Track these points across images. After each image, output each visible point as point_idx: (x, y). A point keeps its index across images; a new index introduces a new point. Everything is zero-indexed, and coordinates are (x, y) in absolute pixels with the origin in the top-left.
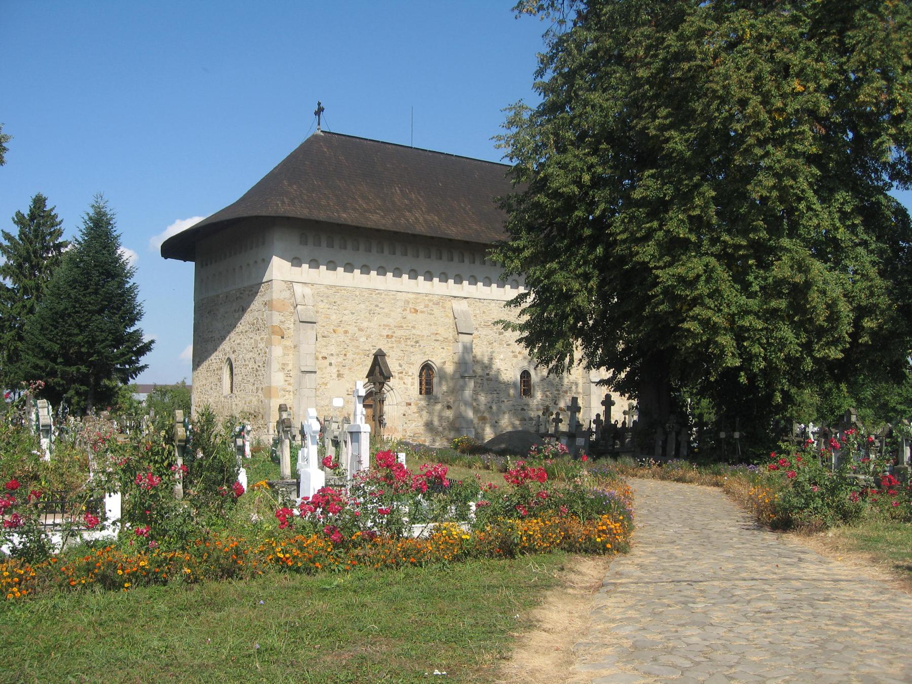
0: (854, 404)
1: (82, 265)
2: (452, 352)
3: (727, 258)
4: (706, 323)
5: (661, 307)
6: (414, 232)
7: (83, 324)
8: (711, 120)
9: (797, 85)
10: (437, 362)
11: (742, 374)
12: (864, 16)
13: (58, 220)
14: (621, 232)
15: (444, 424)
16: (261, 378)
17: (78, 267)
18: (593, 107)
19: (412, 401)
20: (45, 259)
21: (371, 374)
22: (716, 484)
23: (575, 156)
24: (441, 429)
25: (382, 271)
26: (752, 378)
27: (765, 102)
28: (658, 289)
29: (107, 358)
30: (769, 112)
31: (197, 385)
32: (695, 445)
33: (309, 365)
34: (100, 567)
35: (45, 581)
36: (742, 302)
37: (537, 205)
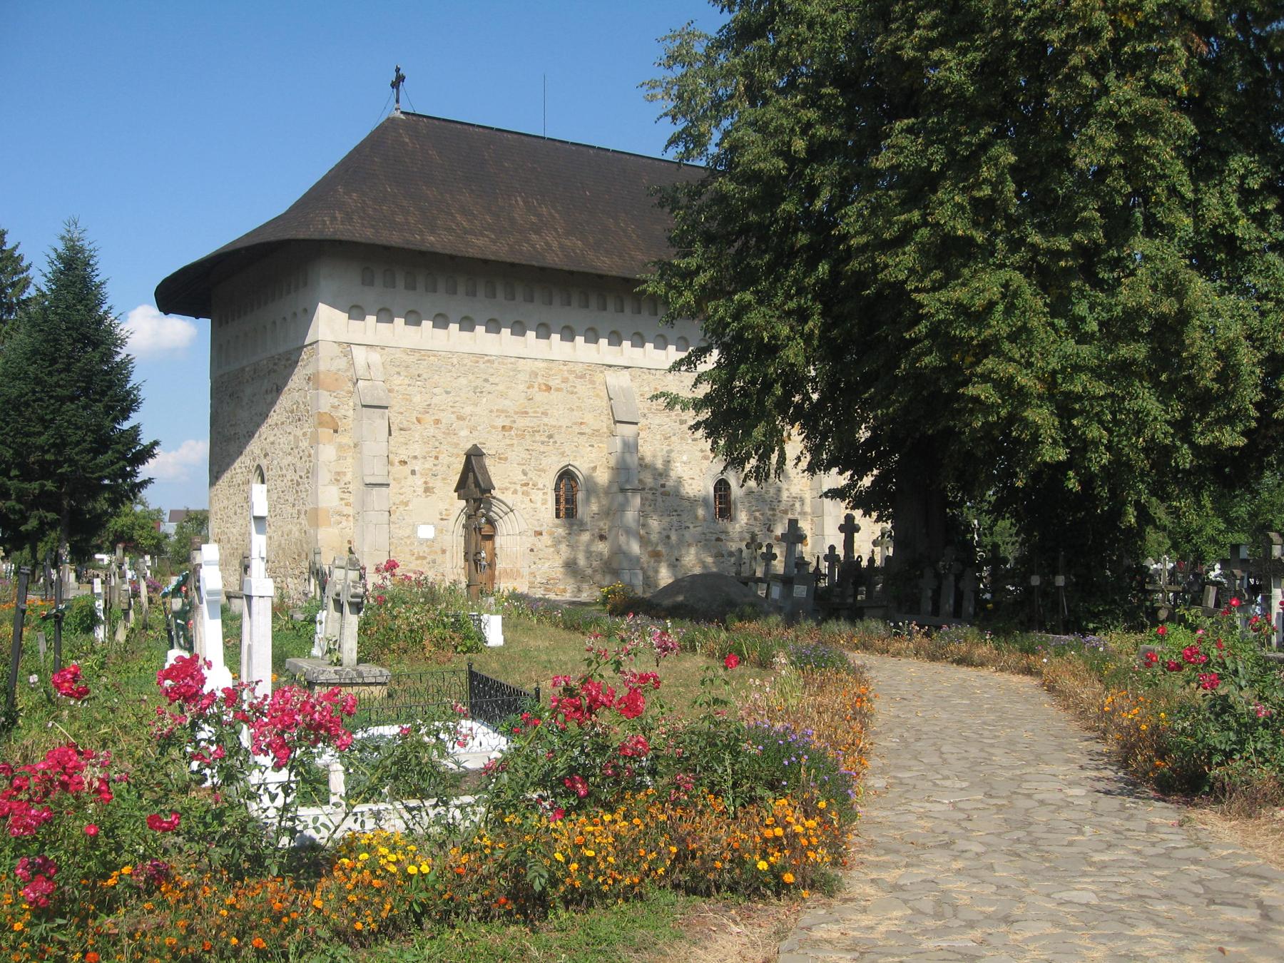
0: (1222, 526)
2: (605, 451)
3: (1045, 275)
4: (1005, 386)
5: (927, 360)
6: (541, 264)
7: (48, 417)
10: (582, 466)
11: (1071, 474)
13: (24, 264)
14: (857, 233)
15: (595, 563)
18: (811, 26)
19: (544, 529)
22: (1028, 671)
23: (781, 109)
24: (589, 571)
26: (1088, 481)
28: (922, 328)
31: (216, 507)
32: (988, 596)
33: (377, 472)
37: (722, 198)
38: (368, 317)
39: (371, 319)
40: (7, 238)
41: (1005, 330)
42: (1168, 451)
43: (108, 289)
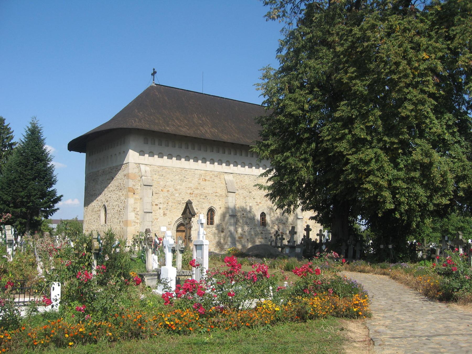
1: (24, 154)
2: (224, 202)
3: (386, 150)
4: (376, 185)
5: (351, 176)
8: (379, 73)
9: (425, 55)
12: (459, 19)
13: (11, 131)
16: (122, 215)
17: (22, 155)
18: (310, 68)
20: (4, 151)
21: (184, 213)
22: (384, 274)
25: (188, 159)
27: (409, 63)
28: (349, 166)
29: (37, 204)
30: (411, 69)
31: (86, 219)
34: (54, 334)
35: (17, 342)
36: (395, 173)
37: (278, 121)
38: (146, 155)
39: (147, 156)
40: (5, 121)
41: (376, 167)
42: (426, 205)
43: (45, 141)
